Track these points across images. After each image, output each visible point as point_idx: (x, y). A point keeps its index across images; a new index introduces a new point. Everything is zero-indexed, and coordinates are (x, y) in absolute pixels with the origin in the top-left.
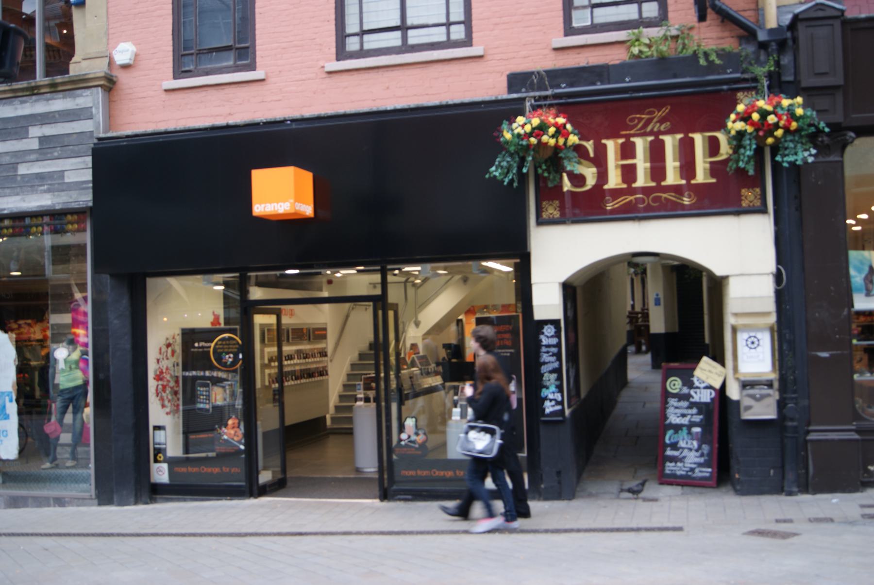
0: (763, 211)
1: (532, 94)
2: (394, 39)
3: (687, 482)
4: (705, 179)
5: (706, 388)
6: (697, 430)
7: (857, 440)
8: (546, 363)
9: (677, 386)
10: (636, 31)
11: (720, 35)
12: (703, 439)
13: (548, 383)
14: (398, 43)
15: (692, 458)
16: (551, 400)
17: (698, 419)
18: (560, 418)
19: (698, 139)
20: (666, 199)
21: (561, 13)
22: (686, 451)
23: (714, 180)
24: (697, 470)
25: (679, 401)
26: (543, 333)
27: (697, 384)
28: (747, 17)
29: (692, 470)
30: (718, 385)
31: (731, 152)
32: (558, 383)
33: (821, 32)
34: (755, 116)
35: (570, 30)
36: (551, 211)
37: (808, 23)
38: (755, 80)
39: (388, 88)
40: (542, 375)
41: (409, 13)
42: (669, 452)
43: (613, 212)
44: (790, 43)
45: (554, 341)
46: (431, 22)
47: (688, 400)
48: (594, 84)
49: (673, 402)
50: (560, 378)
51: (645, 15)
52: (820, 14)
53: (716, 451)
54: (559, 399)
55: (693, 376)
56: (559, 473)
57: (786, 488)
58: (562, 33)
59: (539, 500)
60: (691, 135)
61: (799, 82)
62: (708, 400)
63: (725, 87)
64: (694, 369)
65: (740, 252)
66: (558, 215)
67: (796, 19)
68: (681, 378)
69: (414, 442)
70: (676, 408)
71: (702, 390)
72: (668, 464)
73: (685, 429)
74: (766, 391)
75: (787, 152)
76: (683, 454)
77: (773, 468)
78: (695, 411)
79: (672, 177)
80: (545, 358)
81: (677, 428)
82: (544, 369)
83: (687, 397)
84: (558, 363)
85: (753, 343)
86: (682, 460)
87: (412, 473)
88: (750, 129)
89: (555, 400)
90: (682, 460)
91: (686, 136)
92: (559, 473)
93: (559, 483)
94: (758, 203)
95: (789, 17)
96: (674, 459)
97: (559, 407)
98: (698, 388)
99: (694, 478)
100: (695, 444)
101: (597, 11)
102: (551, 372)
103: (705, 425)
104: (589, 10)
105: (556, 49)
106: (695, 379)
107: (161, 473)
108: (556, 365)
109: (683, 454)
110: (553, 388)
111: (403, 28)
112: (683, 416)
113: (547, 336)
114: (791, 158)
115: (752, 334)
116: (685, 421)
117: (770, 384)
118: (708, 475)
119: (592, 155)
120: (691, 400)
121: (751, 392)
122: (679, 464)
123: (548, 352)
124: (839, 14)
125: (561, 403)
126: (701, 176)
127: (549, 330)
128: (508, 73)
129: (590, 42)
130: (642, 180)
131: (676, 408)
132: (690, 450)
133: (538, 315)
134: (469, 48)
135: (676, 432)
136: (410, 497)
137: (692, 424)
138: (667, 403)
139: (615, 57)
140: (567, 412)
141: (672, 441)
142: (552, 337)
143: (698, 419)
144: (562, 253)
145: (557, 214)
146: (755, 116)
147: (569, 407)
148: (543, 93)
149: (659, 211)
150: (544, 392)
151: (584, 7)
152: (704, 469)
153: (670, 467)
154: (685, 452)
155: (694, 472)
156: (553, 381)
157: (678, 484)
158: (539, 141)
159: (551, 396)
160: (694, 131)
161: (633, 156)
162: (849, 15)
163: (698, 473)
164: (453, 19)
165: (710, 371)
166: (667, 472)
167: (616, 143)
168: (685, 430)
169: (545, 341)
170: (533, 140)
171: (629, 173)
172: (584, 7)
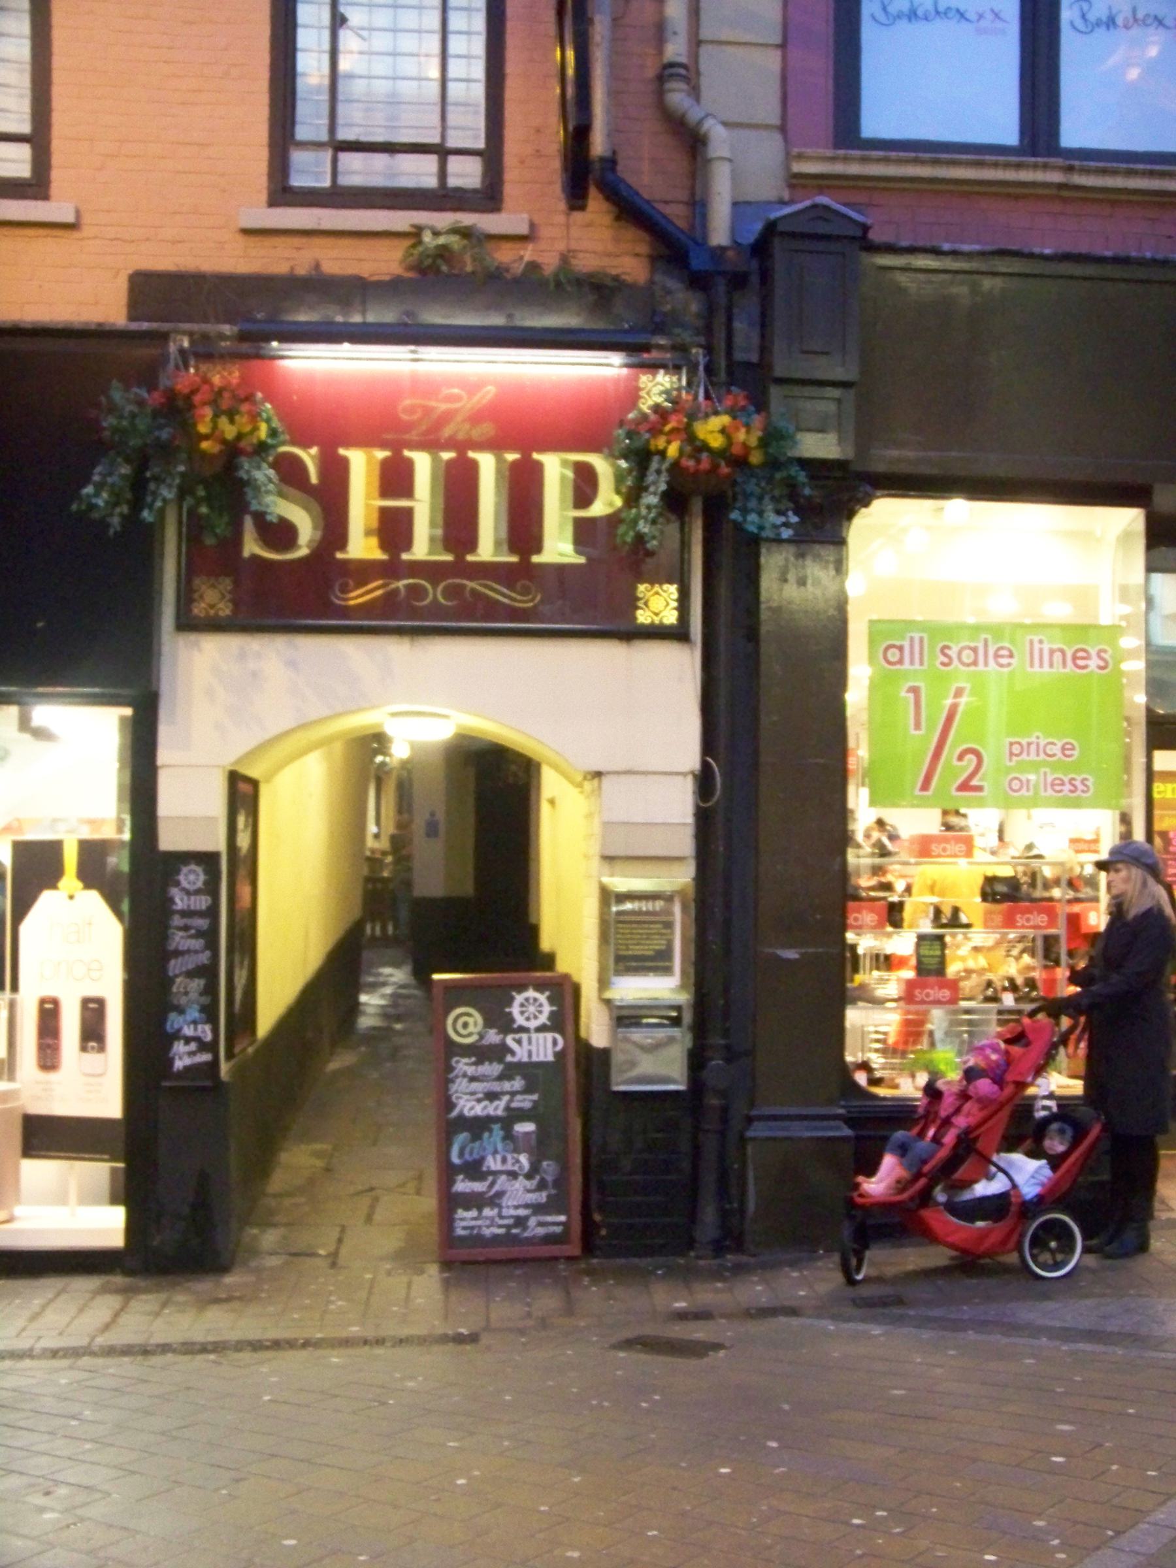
4: (430, 553)
6: (528, 1127)
9: (471, 1029)
11: (610, 247)
12: (540, 1148)
13: (183, 1000)
15: (519, 1194)
16: (188, 1040)
18: (208, 1083)
20: (474, 592)
21: (264, 153)
22: (503, 1177)
24: (532, 1222)
25: (478, 1063)
26: (178, 884)
28: (676, 214)
29: (520, 1222)
31: (618, 502)
32: (206, 1000)
36: (213, 598)
37: (796, 244)
40: (171, 981)
43: (367, 610)
44: (755, 279)
45: (203, 902)
47: (501, 1060)
49: (463, 1065)
50: (211, 990)
51: (452, 182)
52: (822, 228)
54: (209, 1037)
58: (264, 197)
60: (536, 456)
61: (770, 367)
62: (550, 1058)
66: (228, 612)
67: (771, 228)
68: (479, 1010)
70: (473, 1079)
71: (534, 1036)
72: (461, 1213)
73: (496, 1127)
76: (497, 1188)
78: (518, 1084)
80: (179, 940)
82: (175, 966)
83: (499, 1052)
84: (208, 953)
86: (494, 1200)
89: (197, 1039)
90: (494, 1200)
95: (758, 227)
96: (475, 1201)
97: (206, 1057)
98: (522, 1029)
99: (530, 1241)
100: (524, 1159)
101: (350, 160)
102: (190, 974)
104: (328, 155)
105: (247, 232)
108: (204, 958)
109: (497, 1188)
110: (194, 1013)
112: (492, 1096)
116: (497, 1108)
118: (558, 1229)
119: (314, 479)
120: (509, 1058)
122: (487, 1212)
123: (186, 928)
124: (859, 233)
125: (212, 1047)
126: (558, 547)
127: (191, 877)
128: (130, 271)
129: (326, 225)
130: (423, 546)
131: (473, 1079)
132: (513, 1175)
133: (169, 840)
134: (40, 203)
135: (477, 1137)
137: (514, 1115)
138: (450, 1069)
140: (224, 1067)
141: (476, 1156)
142: (198, 892)
147: (230, 1055)
150: (174, 1021)
151: (318, 145)
152: (549, 1219)
154: (502, 1182)
155: (525, 1228)
156: (193, 995)
159: (188, 1031)
163: (534, 1228)
166: (460, 1232)
167: (370, 460)
168: (497, 1131)
169: (180, 902)
171: (394, 529)
172: (318, 145)
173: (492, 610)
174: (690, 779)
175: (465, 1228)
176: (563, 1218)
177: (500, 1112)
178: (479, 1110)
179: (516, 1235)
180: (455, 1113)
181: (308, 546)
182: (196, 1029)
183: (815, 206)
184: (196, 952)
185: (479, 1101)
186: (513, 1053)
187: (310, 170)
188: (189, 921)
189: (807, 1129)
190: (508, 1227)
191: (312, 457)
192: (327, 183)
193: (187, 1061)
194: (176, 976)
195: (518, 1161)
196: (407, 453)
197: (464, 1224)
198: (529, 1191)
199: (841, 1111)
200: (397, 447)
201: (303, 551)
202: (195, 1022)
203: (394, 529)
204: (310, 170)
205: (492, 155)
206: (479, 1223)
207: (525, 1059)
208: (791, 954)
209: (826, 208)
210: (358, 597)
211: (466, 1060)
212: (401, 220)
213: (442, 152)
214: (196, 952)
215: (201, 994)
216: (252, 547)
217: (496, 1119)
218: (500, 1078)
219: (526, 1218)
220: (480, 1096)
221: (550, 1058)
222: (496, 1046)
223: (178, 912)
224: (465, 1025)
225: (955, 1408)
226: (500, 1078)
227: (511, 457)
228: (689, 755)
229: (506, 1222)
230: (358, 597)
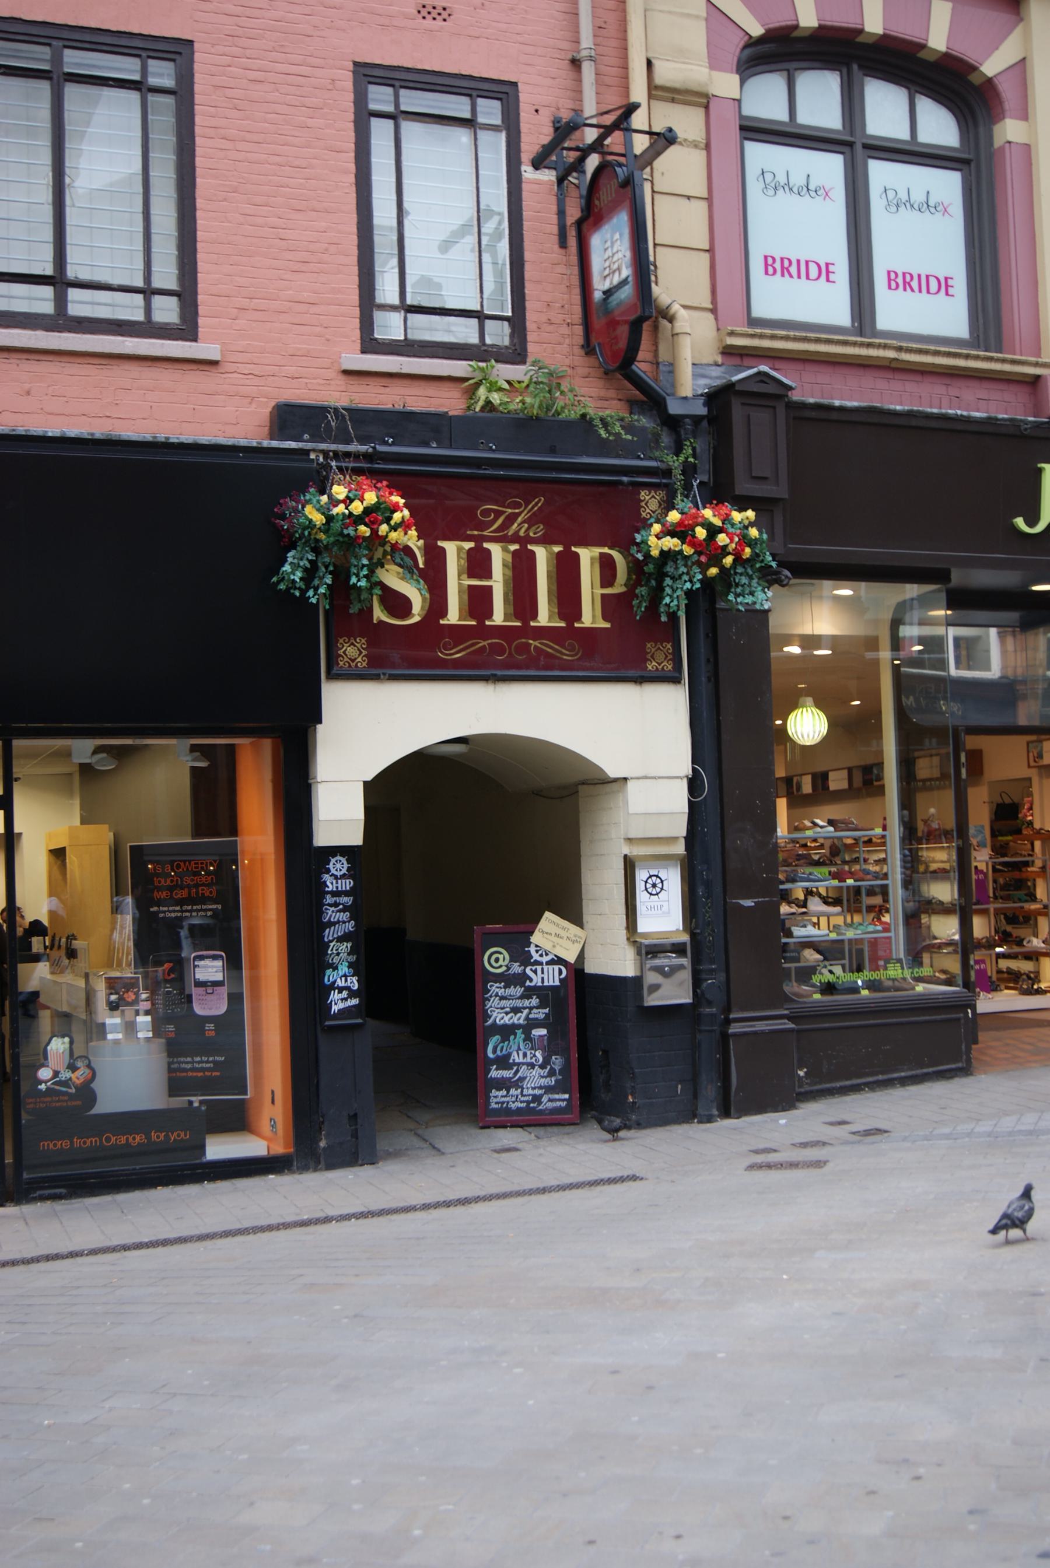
0: (676, 680)
1: (323, 446)
2: (40, 300)
3: (531, 1119)
4: (504, 621)
5: (550, 963)
7: (791, 1030)
8: (334, 924)
9: (501, 962)
10: (483, 365)
11: (603, 393)
12: (551, 1048)
14: (47, 308)
15: (535, 1079)
16: (341, 990)
17: (540, 1014)
19: (587, 556)
22: (524, 1067)
23: (608, 625)
24: (545, 1099)
26: (328, 871)
27: (536, 957)
29: (537, 1099)
30: (571, 958)
33: (761, 417)
34: (701, 533)
35: (370, 345)
38: (668, 473)
39: (28, 393)
41: (73, 255)
42: (494, 1073)
46: (116, 281)
47: (522, 985)
48: (427, 444)
53: (575, 1065)
55: (529, 944)
56: (353, 1118)
57: (701, 1111)
59: (315, 1170)
60: (529, 547)
63: (625, 479)
64: (532, 933)
65: (632, 737)
69: (66, 1083)
70: (502, 998)
71: (545, 968)
72: (494, 1093)
73: (519, 1032)
74: (674, 960)
75: (739, 590)
77: (680, 1082)
78: (535, 1001)
79: (545, 616)
80: (331, 914)
81: (507, 1032)
82: (329, 934)
85: (654, 885)
86: (518, 1083)
87: (64, 1144)
88: (688, 550)
92: (353, 1118)
93: (355, 1135)
94: (669, 666)
96: (504, 1084)
100: (539, 1054)
101: (415, 319)
102: (341, 939)
103: (553, 1023)
105: (347, 373)
106: (532, 949)
110: (344, 969)
111: (59, 281)
112: (516, 1010)
113: (337, 876)
114: (749, 599)
115: (654, 872)
116: (520, 1019)
117: (678, 949)
120: (528, 983)
121: (657, 962)
122: (513, 1091)
123: (336, 905)
126: (590, 617)
127: (339, 866)
131: (502, 998)
133: (323, 838)
135: (505, 1038)
136: (63, 1191)
137: (531, 1024)
139: (448, 402)
141: (504, 1052)
143: (540, 1014)
144: (370, 730)
145: (362, 662)
146: (701, 533)
148: (342, 448)
149: (528, 668)
150: (330, 976)
151: (393, 308)
152: (557, 1096)
153: (497, 1097)
155: (540, 1103)
156: (344, 955)
157: (514, 1126)
158: (375, 532)
159: (341, 983)
161: (489, 575)
162: (795, 396)
163: (546, 1104)
164: (157, 283)
165: (557, 935)
166: (493, 1106)
167: (550, 553)
169: (331, 885)
170: (364, 530)
171: (478, 601)
174: (685, 781)
175: (497, 1103)
176: (567, 1096)
177: (521, 1021)
178: (507, 1020)
179: (534, 1108)
180: (490, 1022)
182: (346, 981)
183: (759, 373)
184: (344, 922)
185: (507, 1013)
186: (531, 980)
187: (391, 327)
188: (337, 899)
189: (767, 1025)
190: (528, 1102)
191: (419, 548)
192: (402, 338)
193: (341, 1005)
194: (331, 941)
195: (535, 1056)
196: (486, 545)
197: (498, 1100)
198: (542, 1077)
199: (786, 1012)
200: (479, 540)
202: (345, 976)
203: (478, 601)
204: (391, 327)
205: (517, 321)
206: (507, 1099)
207: (539, 984)
208: (748, 903)
209: (766, 374)
211: (497, 985)
212: (458, 368)
213: (479, 316)
214: (344, 922)
215: (349, 954)
216: (379, 614)
217: (519, 1026)
218: (522, 997)
219: (541, 1096)
220: (508, 1010)
221: (557, 983)
222: (519, 974)
224: (497, 960)
226: (522, 997)
227: (557, 549)
228: (685, 767)
229: (526, 1099)
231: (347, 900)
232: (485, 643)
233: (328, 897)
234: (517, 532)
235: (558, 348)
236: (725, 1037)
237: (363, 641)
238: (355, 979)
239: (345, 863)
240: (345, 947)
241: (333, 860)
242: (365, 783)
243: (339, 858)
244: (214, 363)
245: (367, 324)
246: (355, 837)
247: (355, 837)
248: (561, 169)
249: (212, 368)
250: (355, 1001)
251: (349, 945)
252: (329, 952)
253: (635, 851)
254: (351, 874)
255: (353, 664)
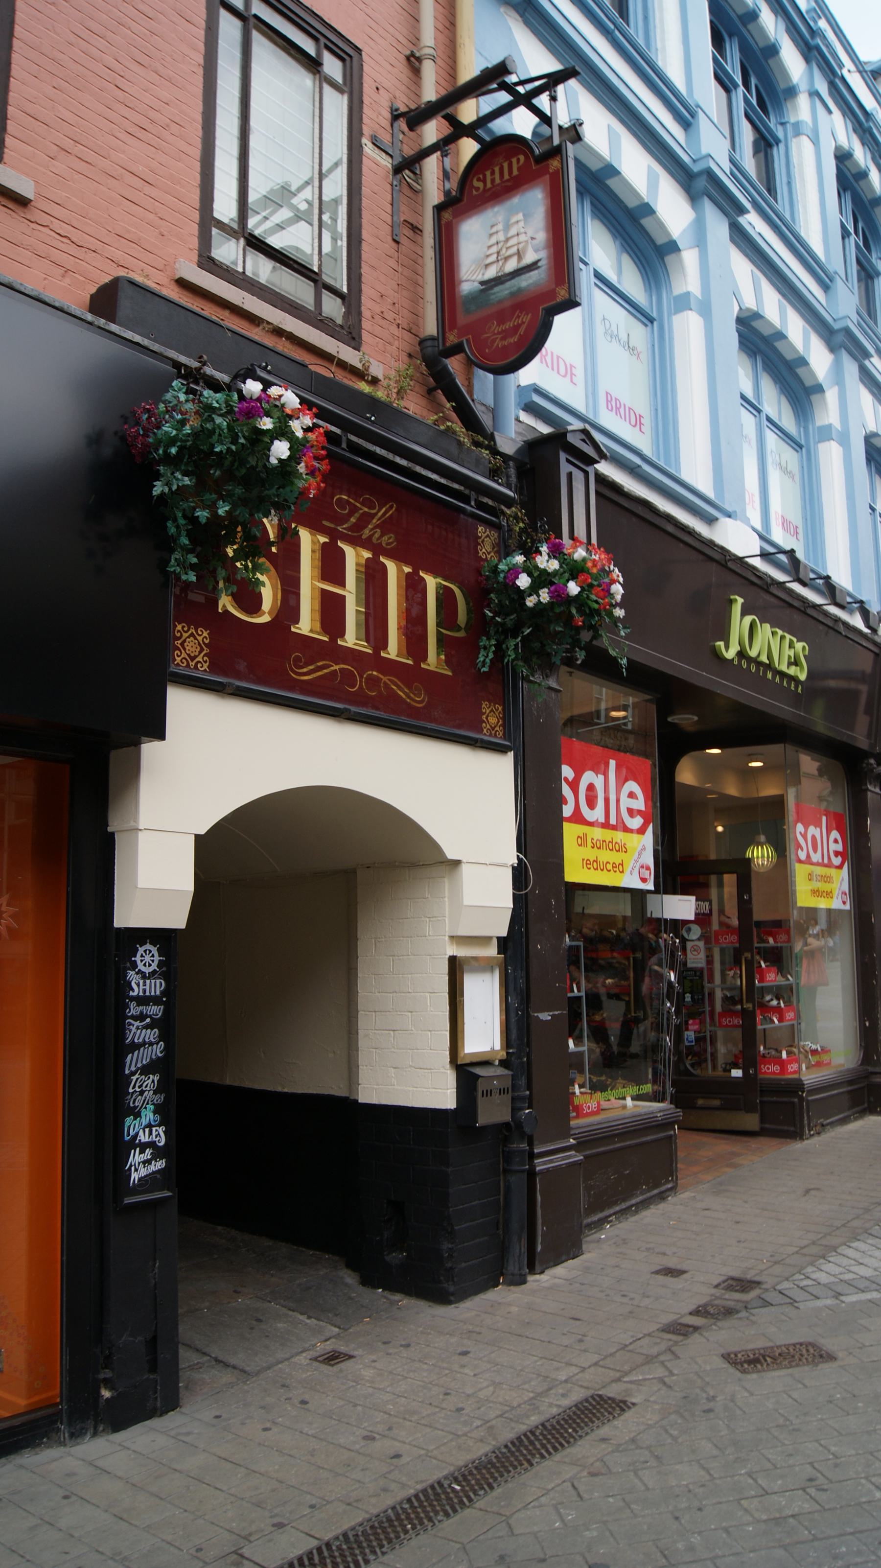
16: (143, 1147)
26: (134, 965)
35: (208, 263)
40: (127, 1080)
80: (136, 1032)
82: (133, 1062)
89: (152, 1145)
91: (415, 572)
102: (146, 1070)
107: (687, 774)
110: (148, 1115)
123: (141, 1017)
127: (148, 958)
130: (351, 637)
133: (127, 915)
156: (149, 1095)
159: (144, 1138)
160: (428, 571)
161: (342, 583)
171: (331, 610)
173: (389, 701)
181: (269, 613)
182: (151, 1133)
184: (151, 1044)
193: (143, 1172)
194: (133, 1074)
200: (334, 536)
201: (265, 619)
202: (150, 1126)
210: (307, 674)
214: (151, 1044)
215: (155, 1093)
216: (226, 603)
223: (133, 999)
225: (479, 1408)
230: (307, 674)
231: (156, 1010)
232: (336, 667)
233: (133, 1005)
234: (370, 538)
235: (389, 347)
236: (532, 1174)
237: (205, 634)
238: (161, 1130)
239: (156, 954)
240: (152, 1081)
241: (141, 950)
242: (197, 837)
243: (148, 946)
244: (22, 202)
245: (205, 241)
246: (176, 917)
247: (176, 917)
248: (398, 160)
249: (20, 210)
250: (160, 1164)
251: (156, 1078)
252: (131, 1090)
253: (461, 952)
254: (166, 971)
255: (192, 664)
